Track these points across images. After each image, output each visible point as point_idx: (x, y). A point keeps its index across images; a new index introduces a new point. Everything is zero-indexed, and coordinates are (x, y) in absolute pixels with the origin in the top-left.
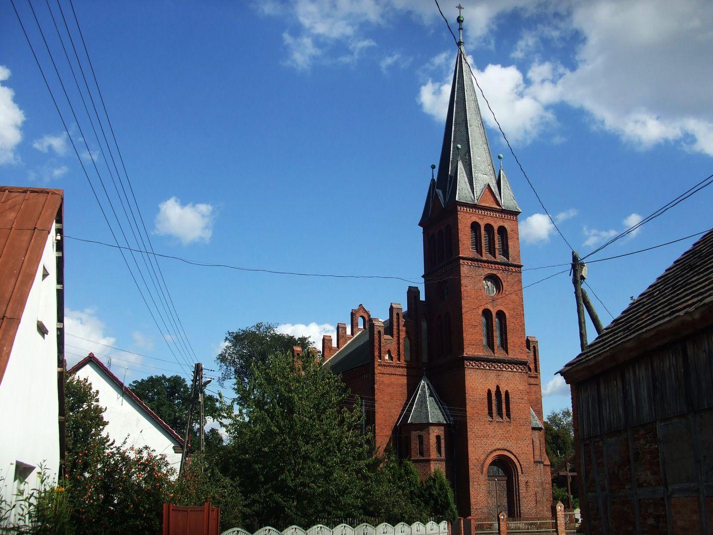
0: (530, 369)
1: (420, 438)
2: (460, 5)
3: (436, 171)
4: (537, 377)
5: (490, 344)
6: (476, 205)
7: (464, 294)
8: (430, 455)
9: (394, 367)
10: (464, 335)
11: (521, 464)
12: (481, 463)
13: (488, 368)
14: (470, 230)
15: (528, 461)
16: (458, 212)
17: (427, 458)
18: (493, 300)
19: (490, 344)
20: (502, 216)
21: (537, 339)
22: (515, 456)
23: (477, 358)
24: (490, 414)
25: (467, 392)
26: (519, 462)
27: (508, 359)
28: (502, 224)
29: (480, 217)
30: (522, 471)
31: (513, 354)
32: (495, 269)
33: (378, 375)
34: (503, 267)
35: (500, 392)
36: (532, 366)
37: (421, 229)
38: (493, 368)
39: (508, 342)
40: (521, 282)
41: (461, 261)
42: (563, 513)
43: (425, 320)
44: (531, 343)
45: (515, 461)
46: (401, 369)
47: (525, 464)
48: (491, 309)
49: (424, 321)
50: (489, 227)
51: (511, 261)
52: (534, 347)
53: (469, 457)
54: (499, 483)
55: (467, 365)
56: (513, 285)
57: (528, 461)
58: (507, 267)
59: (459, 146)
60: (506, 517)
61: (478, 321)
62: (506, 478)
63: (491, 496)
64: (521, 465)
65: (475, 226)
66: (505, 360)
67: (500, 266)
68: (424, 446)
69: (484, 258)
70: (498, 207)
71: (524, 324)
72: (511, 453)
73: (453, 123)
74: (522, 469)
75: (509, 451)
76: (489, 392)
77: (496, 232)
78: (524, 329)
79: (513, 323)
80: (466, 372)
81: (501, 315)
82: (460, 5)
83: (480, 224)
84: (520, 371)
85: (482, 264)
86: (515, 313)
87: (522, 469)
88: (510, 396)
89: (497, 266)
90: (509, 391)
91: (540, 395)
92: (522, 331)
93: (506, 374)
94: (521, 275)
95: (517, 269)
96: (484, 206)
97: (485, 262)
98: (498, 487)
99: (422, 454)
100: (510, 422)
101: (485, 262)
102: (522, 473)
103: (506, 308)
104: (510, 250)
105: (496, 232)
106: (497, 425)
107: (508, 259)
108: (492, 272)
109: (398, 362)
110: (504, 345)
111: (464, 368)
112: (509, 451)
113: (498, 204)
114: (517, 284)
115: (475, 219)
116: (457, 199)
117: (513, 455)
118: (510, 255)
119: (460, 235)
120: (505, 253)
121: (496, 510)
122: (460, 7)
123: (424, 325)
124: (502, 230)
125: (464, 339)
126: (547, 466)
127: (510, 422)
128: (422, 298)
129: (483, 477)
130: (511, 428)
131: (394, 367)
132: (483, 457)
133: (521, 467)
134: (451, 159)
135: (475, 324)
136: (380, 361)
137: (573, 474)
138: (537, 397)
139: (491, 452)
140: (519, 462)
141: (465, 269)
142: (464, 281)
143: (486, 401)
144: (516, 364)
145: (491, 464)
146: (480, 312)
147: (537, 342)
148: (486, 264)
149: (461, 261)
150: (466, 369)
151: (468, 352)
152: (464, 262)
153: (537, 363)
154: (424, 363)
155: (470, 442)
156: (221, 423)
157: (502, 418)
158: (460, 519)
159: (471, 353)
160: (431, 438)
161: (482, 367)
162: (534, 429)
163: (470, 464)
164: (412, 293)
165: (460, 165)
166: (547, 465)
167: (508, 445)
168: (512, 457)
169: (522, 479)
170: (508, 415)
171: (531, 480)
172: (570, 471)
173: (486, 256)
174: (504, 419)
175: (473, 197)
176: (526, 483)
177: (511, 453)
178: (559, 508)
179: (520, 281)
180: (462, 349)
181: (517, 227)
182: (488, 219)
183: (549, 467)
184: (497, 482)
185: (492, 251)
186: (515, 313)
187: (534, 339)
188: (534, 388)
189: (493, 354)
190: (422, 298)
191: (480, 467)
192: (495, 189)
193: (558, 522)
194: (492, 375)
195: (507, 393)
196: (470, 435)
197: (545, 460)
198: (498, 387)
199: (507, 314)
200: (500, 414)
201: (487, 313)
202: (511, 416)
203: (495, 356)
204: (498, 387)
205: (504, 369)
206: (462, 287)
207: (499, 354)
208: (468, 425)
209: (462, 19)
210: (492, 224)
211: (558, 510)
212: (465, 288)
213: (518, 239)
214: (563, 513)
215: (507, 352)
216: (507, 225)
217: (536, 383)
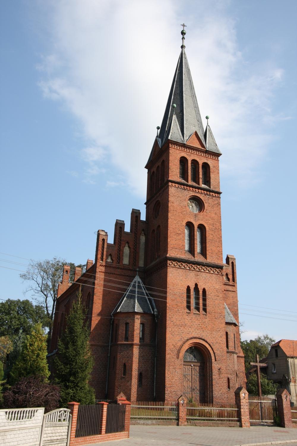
0: (229, 280)
1: (127, 324)
2: (184, 24)
3: (159, 130)
4: (234, 286)
5: (192, 251)
6: (185, 144)
7: (171, 208)
8: (133, 340)
9: (114, 268)
10: (169, 240)
11: (215, 352)
12: (178, 348)
13: (188, 268)
14: (179, 163)
15: (221, 350)
16: (170, 148)
17: (130, 343)
18: (196, 215)
19: (192, 251)
20: (206, 156)
21: (235, 257)
22: (209, 345)
23: (179, 259)
24: (189, 307)
25: (168, 286)
26: (213, 350)
27: (206, 262)
28: (206, 161)
29: (188, 153)
30: (215, 358)
31: (210, 259)
32: (199, 192)
33: (99, 273)
34: (205, 192)
35: (199, 289)
36: (230, 277)
37: (147, 170)
38: (193, 269)
39: (207, 249)
40: (220, 205)
41: (170, 184)
42: (248, 401)
43: (143, 234)
44: (230, 259)
45: (210, 349)
46: (119, 270)
47: (218, 352)
48: (194, 223)
49: (142, 235)
50: (195, 162)
51: (212, 188)
52: (232, 263)
53: (167, 343)
54: (194, 368)
55: (170, 265)
56: (213, 206)
57: (221, 350)
58: (208, 193)
59: (175, 105)
60: (185, 402)
61: (181, 230)
62: (199, 364)
63: (187, 379)
64: (214, 353)
65: (183, 161)
66: (203, 263)
67: (202, 191)
68: (130, 333)
69: (231, 284)
70: (201, 148)
71: (221, 237)
72: (206, 342)
73: (173, 94)
74: (215, 357)
75: (204, 340)
76: (188, 289)
77: (201, 166)
78: (222, 241)
79: (212, 235)
80: (168, 270)
81: (202, 228)
82: (184, 24)
83: (188, 158)
84: (216, 273)
85: (188, 188)
86: (214, 228)
87: (215, 357)
88: (207, 293)
89: (200, 191)
90: (206, 289)
91: (237, 300)
92: (219, 242)
93: (204, 275)
94: (220, 200)
95: (217, 195)
96: (192, 146)
97: (190, 186)
98: (193, 372)
99: (127, 339)
100: (206, 315)
101: (190, 186)
102: (216, 360)
103: (207, 223)
104: (212, 181)
105: (201, 166)
106: (194, 316)
107: (210, 187)
108: (195, 195)
109: (118, 265)
110: (204, 252)
111: (167, 266)
112: (204, 340)
113: (203, 146)
114: (216, 206)
115: (183, 154)
116: (169, 138)
117: (208, 344)
118: (211, 184)
119: (170, 164)
120: (207, 181)
121: (191, 393)
122: (184, 25)
123: (143, 239)
124: (206, 166)
125: (169, 243)
126: (241, 357)
127: (206, 315)
128: (143, 217)
129: (179, 362)
130: (207, 320)
131: (114, 268)
132: (179, 344)
133: (215, 355)
134: (169, 117)
135: (179, 232)
136: (102, 262)
137: (262, 365)
138: (234, 301)
139: (188, 340)
140: (213, 350)
141: (173, 190)
142: (171, 199)
143: (185, 295)
144: (213, 267)
145: (187, 351)
146: (184, 224)
147: (235, 259)
148: (191, 189)
149: (170, 184)
150: (168, 267)
151: (171, 253)
152: (172, 185)
153: (235, 275)
154: (140, 267)
155: (168, 330)
156: (240, 389)
157: (199, 311)
158: (103, 404)
159: (174, 255)
160: (135, 325)
161: (183, 267)
162: (228, 324)
163: (167, 349)
164: (135, 214)
165: (174, 117)
166: (241, 357)
167: (204, 335)
168: (207, 346)
169: (215, 366)
170: (205, 310)
171: (223, 367)
172: (260, 362)
173: (190, 183)
174: (201, 312)
175: (183, 139)
176: (219, 369)
177: (206, 342)
178: (243, 395)
179: (219, 204)
180: (166, 251)
181: (218, 165)
182: (195, 156)
183: (244, 359)
184: (193, 367)
185: (195, 179)
186: (214, 228)
187: (232, 257)
188: (231, 294)
189: (193, 258)
190: (143, 217)
191: (176, 352)
192: (202, 138)
193: (242, 410)
194: (192, 274)
195: (204, 291)
196: (168, 322)
197: (239, 353)
198: (196, 285)
199: (207, 228)
200: (198, 309)
201: (190, 225)
202: (207, 310)
203: (195, 259)
204: (196, 285)
205: (203, 271)
206: (169, 203)
207: (199, 258)
208: (168, 315)
209: (184, 32)
210: (198, 160)
211: (242, 398)
212: (172, 204)
213: (218, 173)
214: (248, 401)
215: (206, 258)
216: (210, 162)
217: (233, 290)
